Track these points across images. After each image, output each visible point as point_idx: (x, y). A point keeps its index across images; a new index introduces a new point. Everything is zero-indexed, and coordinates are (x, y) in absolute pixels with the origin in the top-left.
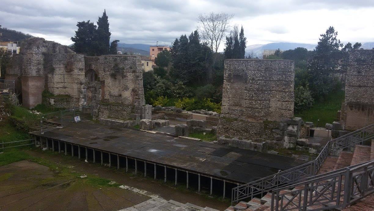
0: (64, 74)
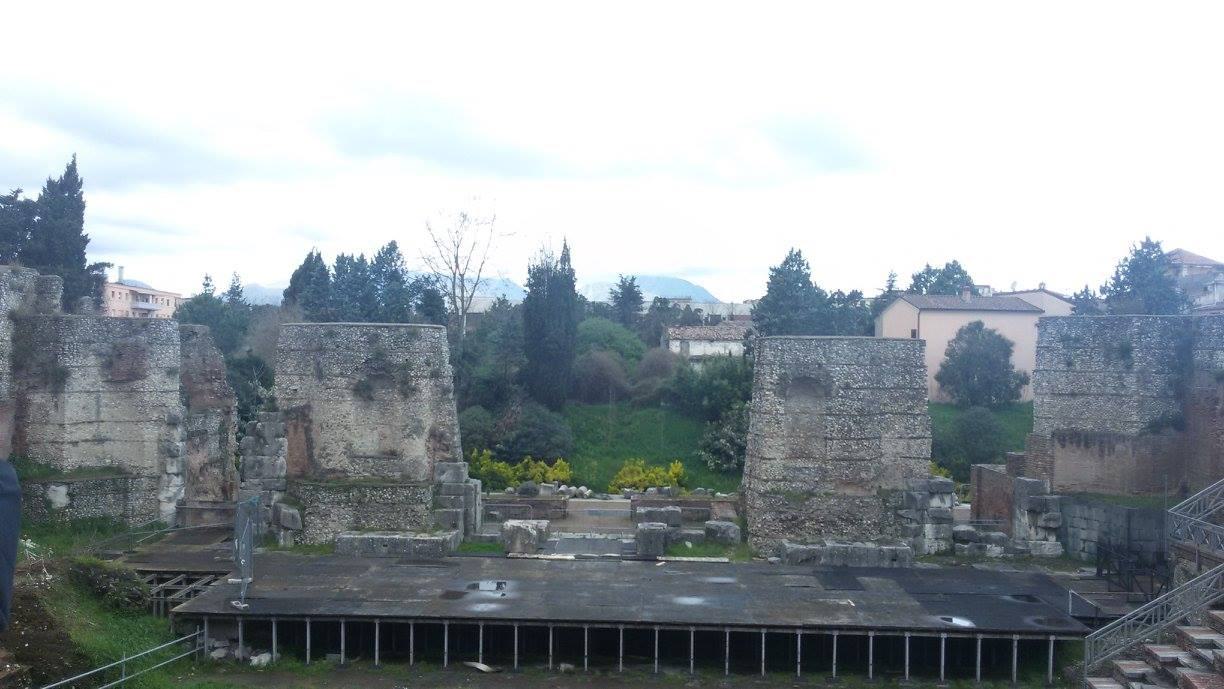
0: (99, 391)
